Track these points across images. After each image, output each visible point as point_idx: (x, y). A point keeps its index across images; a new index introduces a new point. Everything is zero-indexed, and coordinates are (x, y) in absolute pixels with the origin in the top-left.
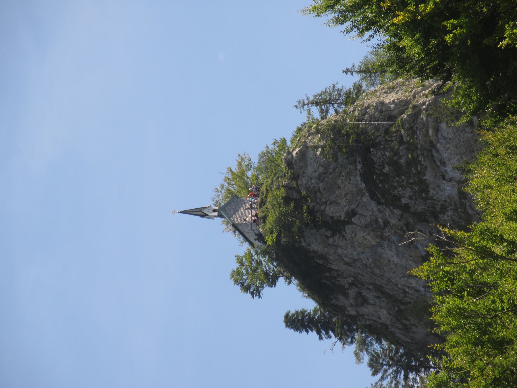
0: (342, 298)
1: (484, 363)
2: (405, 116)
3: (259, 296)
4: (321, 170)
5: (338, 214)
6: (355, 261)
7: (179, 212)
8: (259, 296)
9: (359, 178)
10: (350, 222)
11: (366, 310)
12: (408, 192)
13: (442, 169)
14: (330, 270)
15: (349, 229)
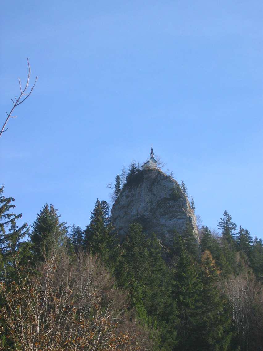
0: (127, 191)
1: (157, 187)
2: (183, 210)
3: (98, 200)
4: (167, 186)
5: (154, 191)
6: (140, 195)
7: (152, 147)
8: (98, 200)
9: (164, 197)
10: (152, 194)
11: (124, 198)
12: (162, 210)
13: (169, 220)
14: (137, 188)
15: (150, 193)
